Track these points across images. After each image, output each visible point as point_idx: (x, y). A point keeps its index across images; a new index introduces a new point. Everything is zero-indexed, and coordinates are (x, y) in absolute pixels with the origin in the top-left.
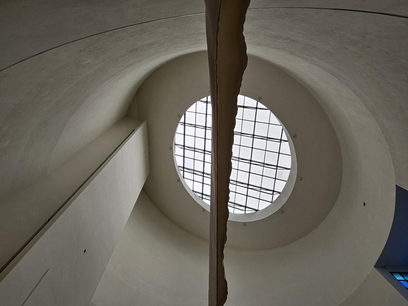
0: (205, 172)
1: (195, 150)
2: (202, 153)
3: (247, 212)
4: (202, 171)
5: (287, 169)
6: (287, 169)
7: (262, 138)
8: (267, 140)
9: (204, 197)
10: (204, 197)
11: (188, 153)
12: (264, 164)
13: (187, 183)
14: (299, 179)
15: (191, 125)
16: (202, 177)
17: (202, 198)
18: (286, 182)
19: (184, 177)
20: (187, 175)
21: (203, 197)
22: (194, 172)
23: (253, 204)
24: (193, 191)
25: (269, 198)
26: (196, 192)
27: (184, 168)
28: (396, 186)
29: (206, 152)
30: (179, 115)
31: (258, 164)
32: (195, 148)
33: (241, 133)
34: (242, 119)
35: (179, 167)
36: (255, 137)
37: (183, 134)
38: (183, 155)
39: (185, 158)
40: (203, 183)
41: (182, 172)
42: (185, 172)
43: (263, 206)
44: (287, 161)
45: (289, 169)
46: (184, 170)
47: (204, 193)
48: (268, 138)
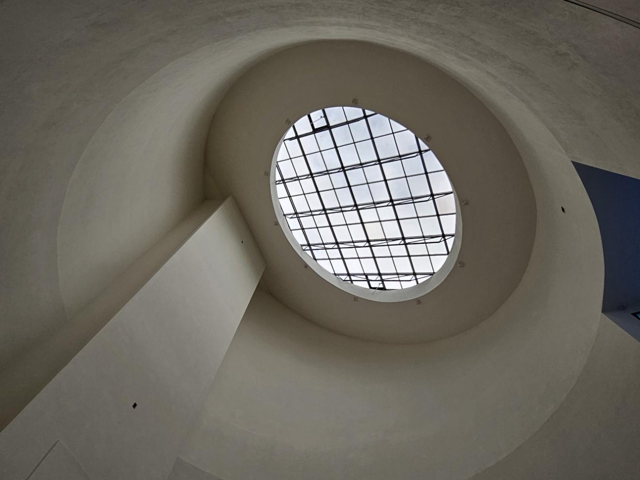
0: (445, 233)
1: (341, 209)
2: (352, 210)
3: (420, 281)
4: (441, 234)
5: (446, 194)
6: (446, 194)
7: (392, 160)
8: (401, 159)
9: (353, 278)
10: (353, 278)
11: (307, 222)
12: (413, 199)
13: (321, 265)
14: (463, 204)
15: (292, 179)
16: (404, 246)
17: (352, 281)
18: (455, 215)
19: (316, 258)
20: (319, 254)
21: (352, 279)
22: (324, 246)
23: (422, 266)
24: (335, 274)
25: (440, 248)
26: (339, 275)
27: (309, 245)
28: (582, 170)
29: (328, 212)
30: (265, 172)
31: (404, 202)
32: (311, 211)
33: (361, 164)
34: (319, 150)
35: (302, 246)
36: (346, 169)
37: (383, 179)
38: (395, 218)
39: (333, 227)
40: (409, 256)
41: (309, 252)
42: (373, 248)
43: (439, 263)
44: (442, 183)
45: (452, 193)
46: (338, 246)
47: (416, 272)
48: (400, 157)
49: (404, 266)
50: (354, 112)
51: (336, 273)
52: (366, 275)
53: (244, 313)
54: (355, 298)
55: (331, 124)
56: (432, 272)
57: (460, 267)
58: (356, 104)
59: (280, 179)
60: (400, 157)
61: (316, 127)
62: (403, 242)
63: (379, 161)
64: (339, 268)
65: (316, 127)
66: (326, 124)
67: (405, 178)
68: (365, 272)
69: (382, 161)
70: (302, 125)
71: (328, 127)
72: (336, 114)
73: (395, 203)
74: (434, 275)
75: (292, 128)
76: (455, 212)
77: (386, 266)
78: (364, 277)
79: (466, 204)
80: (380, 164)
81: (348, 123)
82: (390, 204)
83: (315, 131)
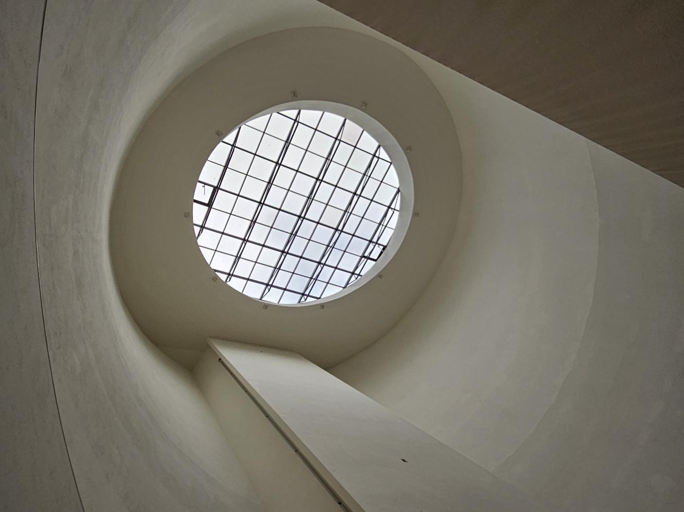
3: (398, 208)
5: (343, 125)
6: (343, 125)
12: (293, 235)
17: (359, 275)
19: (319, 297)
20: (316, 292)
21: (358, 273)
22: (314, 279)
23: (386, 195)
29: (270, 283)
31: (307, 207)
33: (269, 183)
38: (282, 291)
41: (309, 299)
43: (393, 178)
48: (270, 183)
49: (377, 212)
50: (220, 152)
51: (343, 286)
52: (363, 256)
53: (340, 380)
54: (379, 276)
55: (216, 185)
56: (396, 190)
57: (410, 151)
58: (221, 135)
59: (226, 276)
60: (270, 183)
61: (207, 202)
62: (322, 266)
63: (245, 240)
64: (341, 278)
65: (207, 202)
66: (213, 188)
67: (255, 261)
68: (360, 255)
69: (246, 238)
70: (198, 213)
71: (216, 189)
72: (209, 173)
73: (303, 215)
74: (400, 189)
75: (195, 227)
76: (362, 130)
77: (367, 230)
78: (363, 259)
79: (366, 105)
80: (232, 275)
81: (226, 167)
82: (269, 287)
83: (210, 205)
